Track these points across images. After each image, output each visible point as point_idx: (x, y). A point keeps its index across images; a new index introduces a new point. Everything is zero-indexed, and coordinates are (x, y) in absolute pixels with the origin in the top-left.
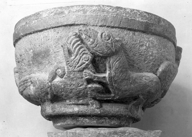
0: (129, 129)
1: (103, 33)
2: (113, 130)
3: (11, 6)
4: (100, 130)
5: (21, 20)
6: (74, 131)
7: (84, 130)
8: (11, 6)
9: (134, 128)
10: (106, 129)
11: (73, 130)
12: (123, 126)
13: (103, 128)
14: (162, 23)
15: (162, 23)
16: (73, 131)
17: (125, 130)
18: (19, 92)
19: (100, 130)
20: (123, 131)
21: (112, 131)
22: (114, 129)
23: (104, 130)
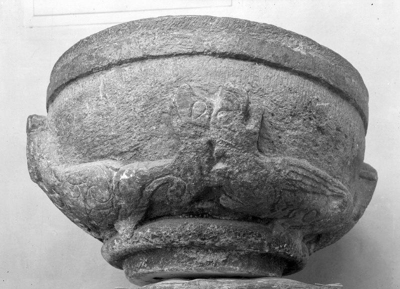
0: (281, 282)
1: (32, 161)
2: (245, 283)
3: (32, 27)
4: (221, 283)
5: (79, 42)
6: (168, 285)
7: (189, 284)
8: (32, 27)
9: (288, 280)
10: (232, 280)
11: (168, 284)
12: (266, 276)
13: (227, 280)
14: (365, 104)
15: (365, 104)
16: (166, 286)
17: (270, 283)
18: (29, 168)
19: (221, 283)
20: (266, 284)
21: (245, 284)
22: (248, 281)
23: (229, 283)
